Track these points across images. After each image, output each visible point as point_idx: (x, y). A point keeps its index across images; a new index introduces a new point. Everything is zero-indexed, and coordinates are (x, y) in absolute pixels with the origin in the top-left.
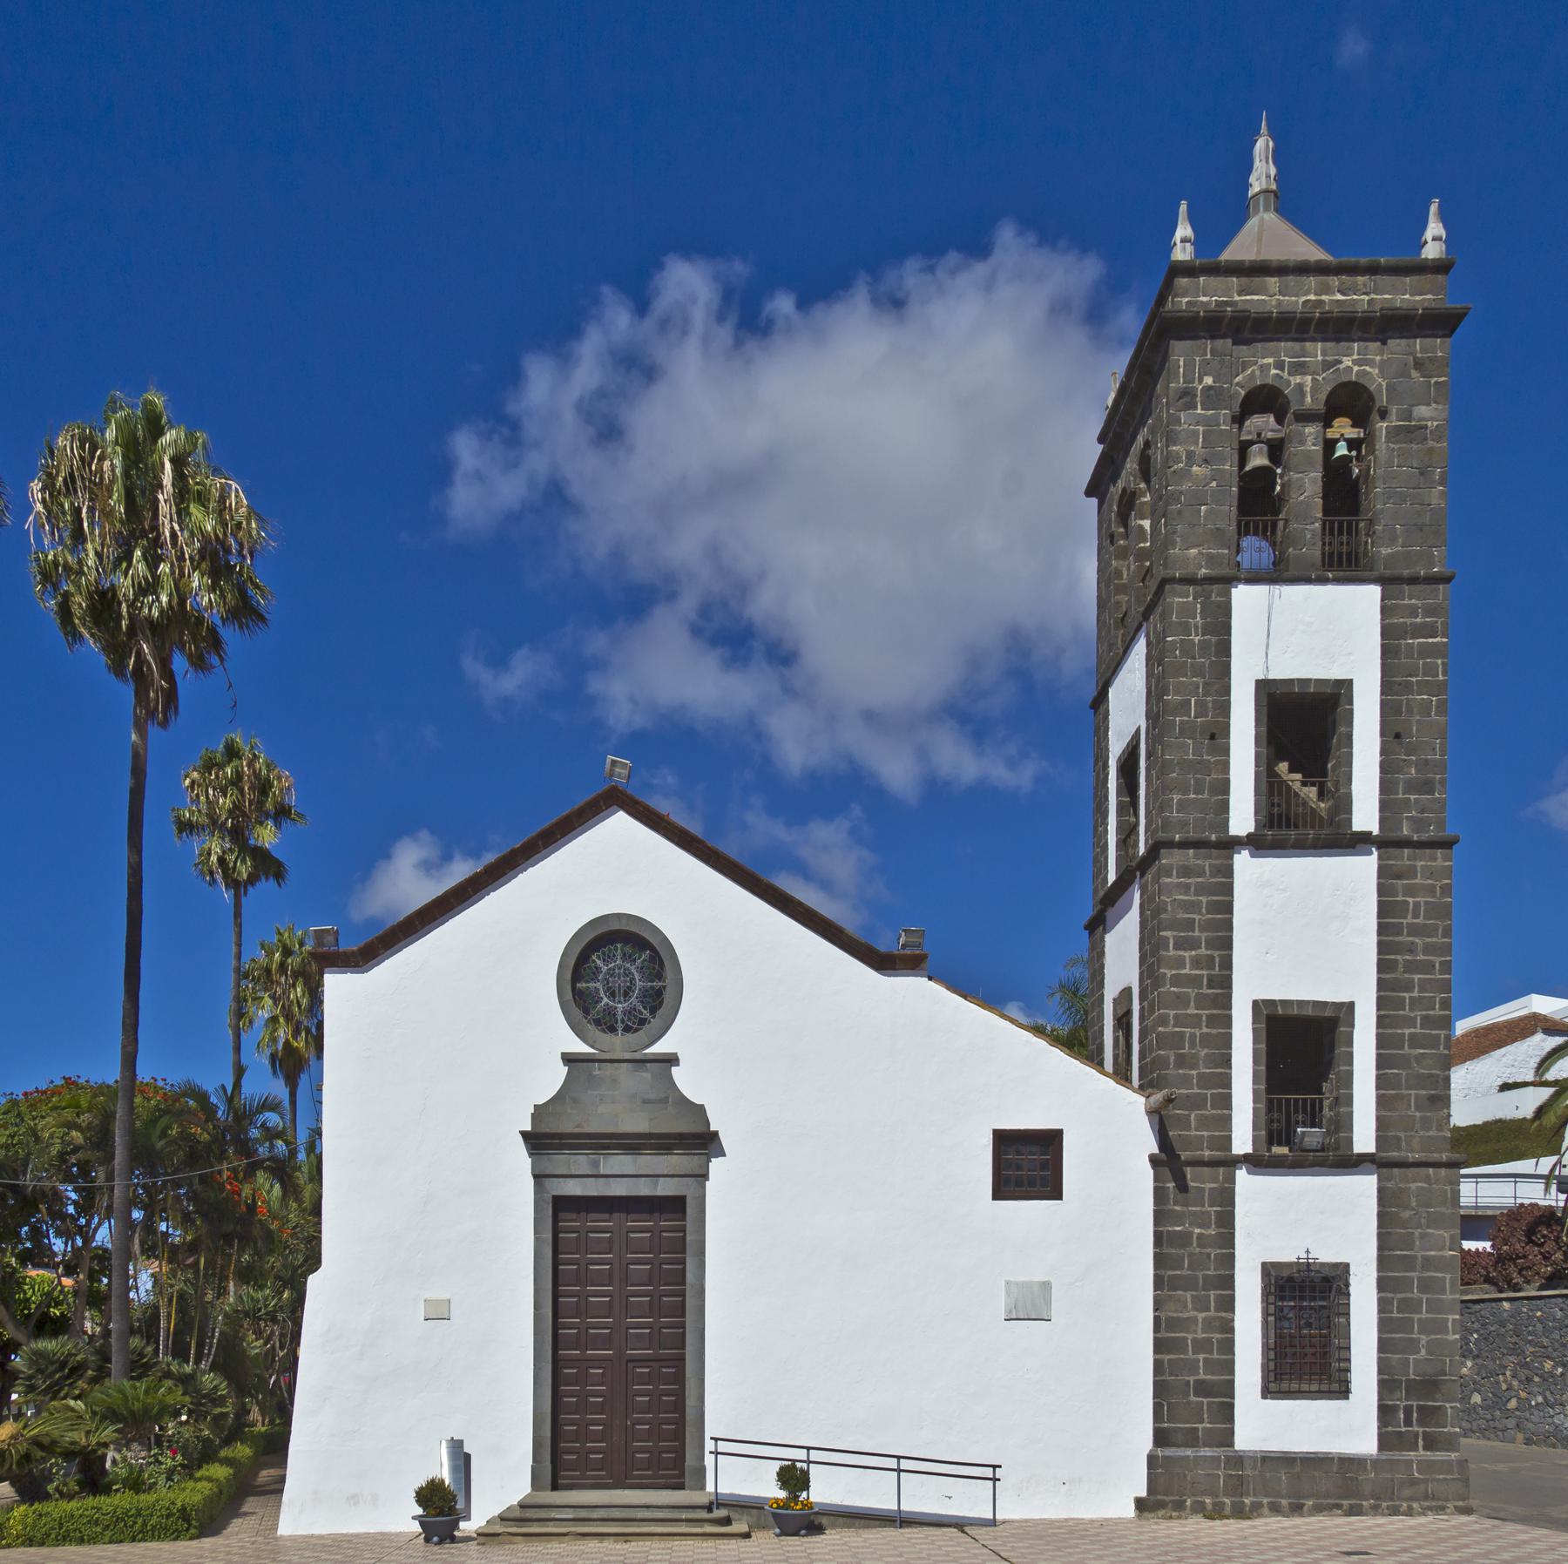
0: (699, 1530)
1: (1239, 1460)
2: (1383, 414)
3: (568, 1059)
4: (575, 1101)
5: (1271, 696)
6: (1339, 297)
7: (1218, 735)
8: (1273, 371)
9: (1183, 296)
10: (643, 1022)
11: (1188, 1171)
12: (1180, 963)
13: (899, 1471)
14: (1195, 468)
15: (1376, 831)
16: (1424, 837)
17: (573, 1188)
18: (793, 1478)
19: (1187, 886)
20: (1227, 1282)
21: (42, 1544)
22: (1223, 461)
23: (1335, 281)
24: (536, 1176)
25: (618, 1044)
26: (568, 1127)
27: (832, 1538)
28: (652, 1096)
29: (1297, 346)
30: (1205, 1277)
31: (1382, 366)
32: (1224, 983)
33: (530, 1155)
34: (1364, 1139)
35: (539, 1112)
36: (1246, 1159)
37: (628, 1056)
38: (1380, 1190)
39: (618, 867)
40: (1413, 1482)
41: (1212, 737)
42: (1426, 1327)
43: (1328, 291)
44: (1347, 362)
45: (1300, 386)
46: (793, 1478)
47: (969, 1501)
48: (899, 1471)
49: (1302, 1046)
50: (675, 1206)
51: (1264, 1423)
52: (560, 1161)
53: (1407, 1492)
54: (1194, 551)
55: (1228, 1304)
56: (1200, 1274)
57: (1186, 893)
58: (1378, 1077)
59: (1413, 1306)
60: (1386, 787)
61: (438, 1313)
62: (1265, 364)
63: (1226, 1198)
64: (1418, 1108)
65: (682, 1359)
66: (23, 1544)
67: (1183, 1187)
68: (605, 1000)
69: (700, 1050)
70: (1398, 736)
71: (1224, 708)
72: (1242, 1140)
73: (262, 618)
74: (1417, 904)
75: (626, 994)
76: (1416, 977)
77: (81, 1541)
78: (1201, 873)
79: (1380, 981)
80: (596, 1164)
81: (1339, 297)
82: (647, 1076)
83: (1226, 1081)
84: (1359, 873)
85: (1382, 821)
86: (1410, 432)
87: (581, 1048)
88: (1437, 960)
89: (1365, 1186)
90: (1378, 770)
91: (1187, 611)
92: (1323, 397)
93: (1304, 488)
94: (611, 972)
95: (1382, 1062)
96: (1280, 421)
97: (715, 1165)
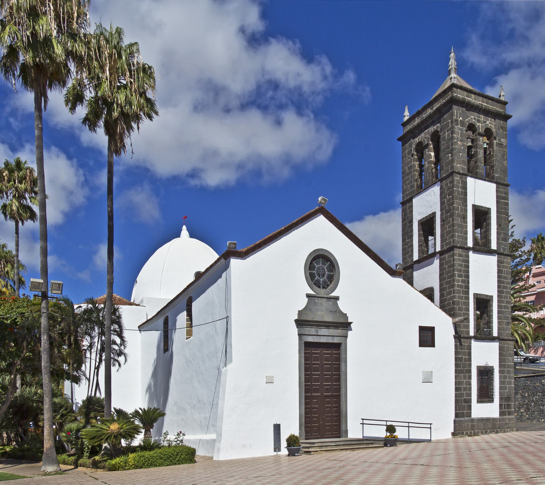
0: (364, 446)
1: (473, 420)
2: (495, 138)
3: (308, 296)
4: (310, 310)
10: (328, 285)
11: (49, 299)
13: (409, 427)
17: (310, 339)
18: (391, 429)
19: (460, 259)
21: (141, 468)
24: (299, 335)
25: (322, 292)
26: (309, 319)
27: (401, 447)
28: (332, 310)
31: (495, 125)
33: (297, 327)
34: (495, 334)
37: (326, 296)
38: (500, 347)
39: (319, 234)
40: (507, 424)
46: (391, 429)
47: (423, 434)
48: (409, 427)
51: (481, 411)
53: (506, 427)
54: (459, 165)
55: (470, 377)
60: (498, 239)
61: (270, 381)
62: (472, 117)
63: (469, 348)
65: (339, 396)
66: (134, 468)
67: (461, 345)
68: (317, 277)
71: (466, 211)
75: (323, 276)
77: (156, 466)
79: (498, 291)
80: (317, 331)
82: (331, 303)
84: (493, 260)
86: (500, 145)
87: (312, 292)
89: (495, 345)
90: (496, 234)
91: (458, 182)
92: (483, 130)
94: (318, 268)
96: (473, 134)
97: (350, 333)
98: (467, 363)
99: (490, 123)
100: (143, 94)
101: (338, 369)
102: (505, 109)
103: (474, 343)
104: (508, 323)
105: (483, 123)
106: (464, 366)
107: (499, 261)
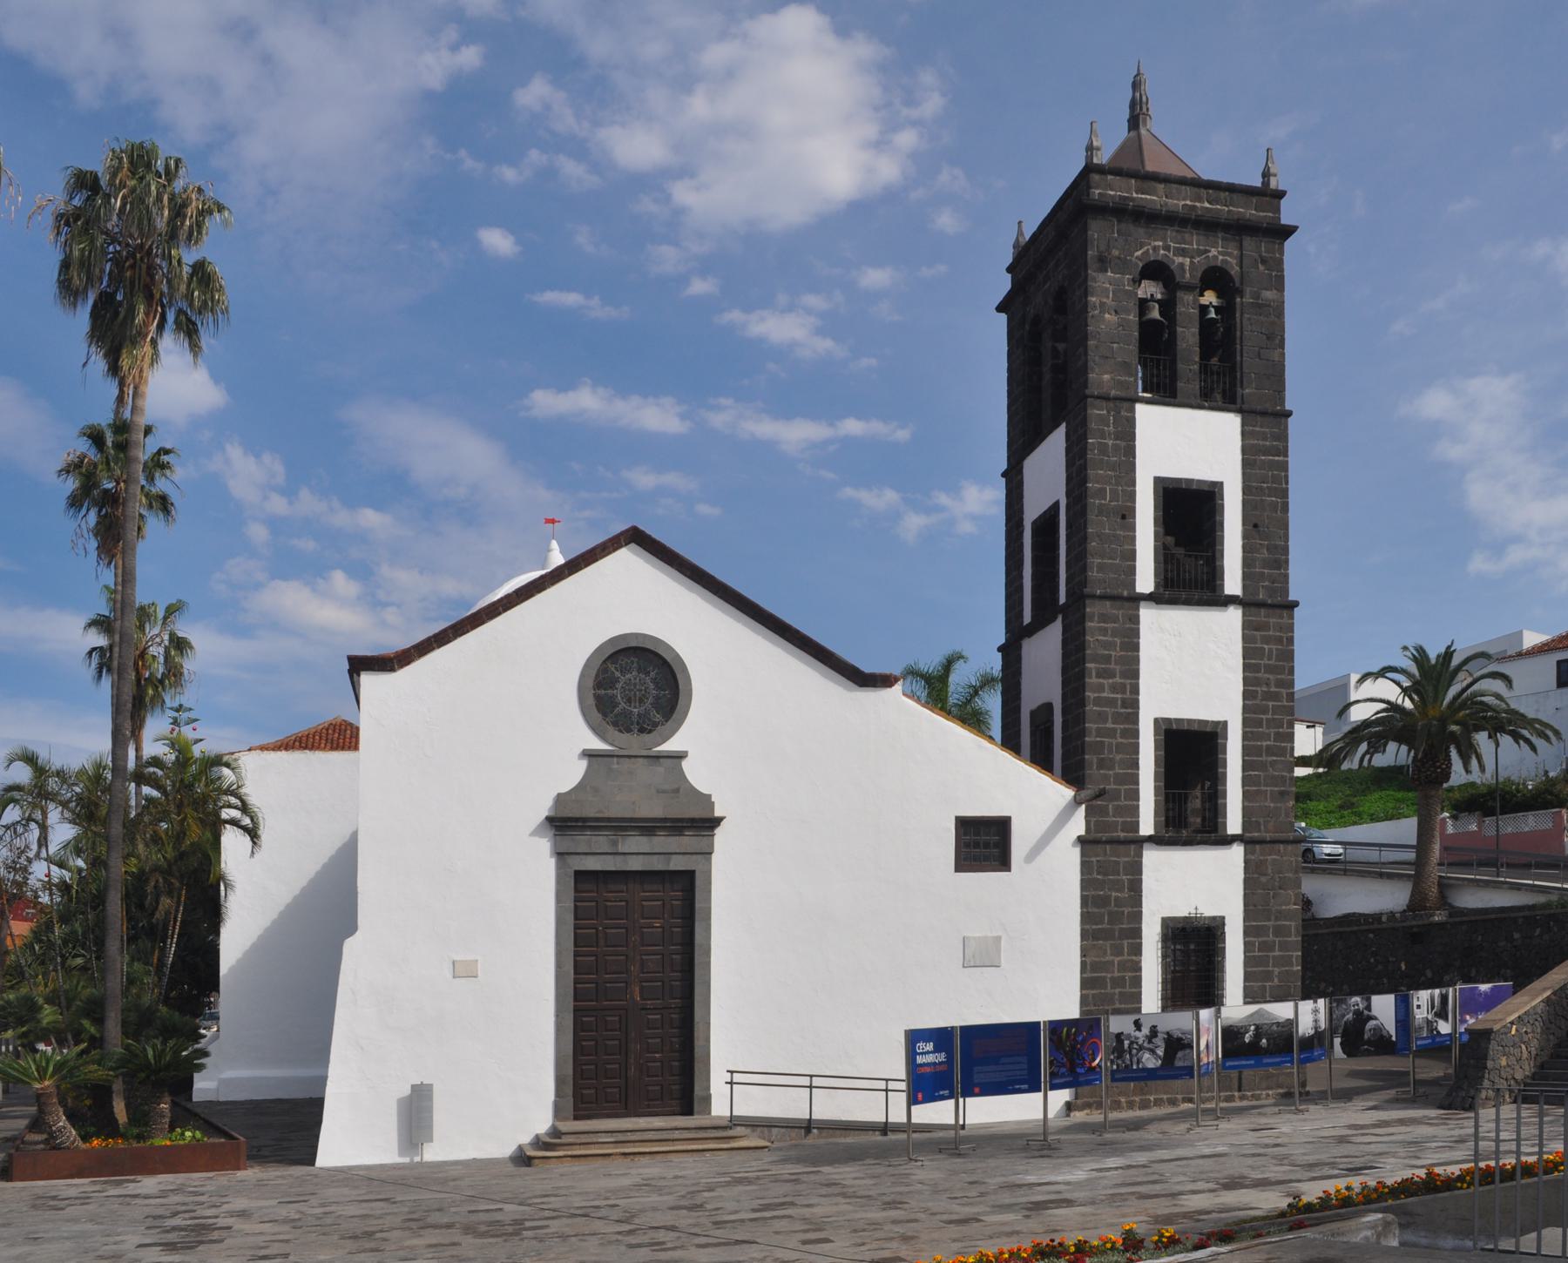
7: (1127, 515)
12: (1101, 688)
20: (1136, 933)
23: (1203, 192)
25: (633, 742)
35: (560, 799)
36: (1150, 839)
41: (1124, 517)
43: (1200, 200)
44: (1213, 252)
45: (1182, 265)
49: (1190, 749)
50: (690, 875)
52: (582, 841)
54: (1106, 377)
55: (1137, 950)
61: (464, 971)
62: (1157, 246)
69: (704, 747)
72: (1147, 827)
75: (641, 701)
80: (615, 843)
87: (598, 744)
88: (1284, 691)
93: (1188, 336)
95: (1246, 766)
99: (1219, 253)
102: (1277, 210)
103: (1151, 619)
104: (1282, 793)
105: (1189, 255)
106: (1115, 918)
107: (1246, 625)
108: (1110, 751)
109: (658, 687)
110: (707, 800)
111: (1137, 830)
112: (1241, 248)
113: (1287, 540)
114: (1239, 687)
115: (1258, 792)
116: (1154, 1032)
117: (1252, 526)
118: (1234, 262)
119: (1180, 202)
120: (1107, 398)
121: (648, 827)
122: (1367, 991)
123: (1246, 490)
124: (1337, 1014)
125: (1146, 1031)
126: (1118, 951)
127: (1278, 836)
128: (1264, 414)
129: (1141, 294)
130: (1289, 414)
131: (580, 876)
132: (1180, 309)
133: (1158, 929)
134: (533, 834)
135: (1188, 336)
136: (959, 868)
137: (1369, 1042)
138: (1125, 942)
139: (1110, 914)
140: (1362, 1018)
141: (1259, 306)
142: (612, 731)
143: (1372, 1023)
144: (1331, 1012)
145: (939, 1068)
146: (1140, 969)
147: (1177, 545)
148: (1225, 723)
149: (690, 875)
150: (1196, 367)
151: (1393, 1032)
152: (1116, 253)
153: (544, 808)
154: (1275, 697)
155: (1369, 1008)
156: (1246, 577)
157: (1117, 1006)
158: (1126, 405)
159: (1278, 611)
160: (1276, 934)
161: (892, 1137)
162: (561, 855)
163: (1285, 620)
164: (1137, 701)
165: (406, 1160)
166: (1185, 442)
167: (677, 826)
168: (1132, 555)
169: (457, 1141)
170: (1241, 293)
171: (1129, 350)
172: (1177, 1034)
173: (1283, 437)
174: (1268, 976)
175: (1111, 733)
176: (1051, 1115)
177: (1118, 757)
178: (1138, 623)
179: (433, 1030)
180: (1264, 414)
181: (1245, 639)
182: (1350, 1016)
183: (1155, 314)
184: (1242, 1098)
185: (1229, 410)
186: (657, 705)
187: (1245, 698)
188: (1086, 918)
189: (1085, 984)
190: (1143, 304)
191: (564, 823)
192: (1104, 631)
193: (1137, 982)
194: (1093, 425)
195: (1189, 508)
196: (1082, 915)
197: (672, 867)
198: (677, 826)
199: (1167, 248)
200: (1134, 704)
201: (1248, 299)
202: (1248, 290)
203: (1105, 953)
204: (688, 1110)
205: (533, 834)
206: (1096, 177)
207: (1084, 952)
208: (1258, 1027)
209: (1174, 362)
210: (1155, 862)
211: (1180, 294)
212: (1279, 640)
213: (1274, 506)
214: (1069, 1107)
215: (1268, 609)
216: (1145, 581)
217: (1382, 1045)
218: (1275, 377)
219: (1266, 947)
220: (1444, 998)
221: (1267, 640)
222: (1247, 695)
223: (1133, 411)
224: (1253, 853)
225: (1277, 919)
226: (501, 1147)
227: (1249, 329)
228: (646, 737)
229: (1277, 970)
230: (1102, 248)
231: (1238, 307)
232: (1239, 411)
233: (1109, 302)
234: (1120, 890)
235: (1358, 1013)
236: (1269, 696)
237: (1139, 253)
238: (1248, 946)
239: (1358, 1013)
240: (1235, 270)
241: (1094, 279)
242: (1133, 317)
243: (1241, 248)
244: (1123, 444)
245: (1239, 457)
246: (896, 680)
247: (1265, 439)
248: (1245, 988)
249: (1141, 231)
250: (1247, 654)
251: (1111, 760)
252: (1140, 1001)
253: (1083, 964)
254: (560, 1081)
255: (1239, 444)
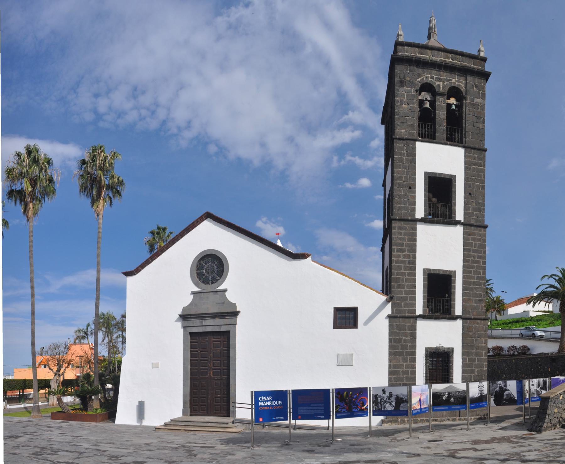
5: (429, 177)
6: (451, 60)
7: (412, 187)
8: (430, 79)
9: (400, 52)
12: (399, 256)
14: (404, 105)
15: (462, 221)
16: (478, 224)
20: (414, 353)
22: (414, 104)
23: (450, 55)
25: (209, 287)
29: (438, 73)
30: (406, 352)
32: (413, 263)
35: (184, 309)
36: (420, 316)
41: (410, 188)
42: (477, 366)
43: (448, 58)
44: (453, 81)
45: (439, 85)
49: (439, 283)
50: (228, 333)
52: (191, 322)
54: (403, 131)
55: (414, 360)
56: (405, 351)
57: (401, 235)
58: (463, 294)
59: (474, 360)
61: (155, 366)
62: (428, 76)
64: (475, 303)
69: (232, 287)
70: (470, 194)
72: (419, 310)
73: (120, 195)
74: (476, 244)
75: (212, 272)
76: (475, 265)
78: (406, 229)
80: (202, 322)
81: (451, 60)
83: (414, 293)
85: (465, 218)
87: (196, 289)
88: (481, 260)
93: (441, 115)
95: (464, 289)
98: (410, 370)
99: (456, 81)
100: (154, 238)
101: (229, 357)
102: (484, 66)
103: (421, 228)
104: (480, 301)
105: (442, 81)
106: (404, 347)
107: (465, 233)
108: (403, 281)
109: (218, 267)
110: (234, 305)
111: (415, 313)
112: (466, 80)
113: (484, 201)
114: (462, 258)
115: (469, 299)
116: (391, 395)
117: (468, 194)
118: (463, 85)
119: (439, 58)
120: (403, 139)
121: (213, 316)
122: (505, 380)
123: (466, 179)
124: (492, 388)
125: (387, 394)
126: (405, 360)
127: (479, 317)
128: (475, 149)
129: (420, 98)
130: (485, 150)
131: (191, 334)
132: (438, 103)
133: (423, 352)
134: (176, 321)
135: (441, 115)
136: (336, 326)
137: (506, 400)
138: (409, 357)
139: (402, 345)
140: (503, 390)
141: (474, 105)
142: (202, 285)
143: (506, 392)
144: (489, 387)
145: (279, 407)
146: (415, 368)
147: (434, 197)
148: (455, 272)
149: (228, 333)
150: (445, 128)
151: (516, 396)
152: (408, 79)
153: (180, 312)
154: (478, 262)
155: (506, 386)
156: (465, 214)
157: (405, 382)
158: (412, 142)
159: (479, 228)
160: (476, 355)
161: (298, 431)
162: (184, 327)
163: (482, 232)
164: (415, 261)
165: (139, 424)
166: (438, 158)
167: (223, 315)
168: (414, 203)
169: (155, 419)
170: (465, 98)
171: (414, 120)
172: (400, 396)
173: (483, 159)
174: (472, 372)
175: (404, 274)
176: (372, 424)
177: (407, 284)
178: (416, 230)
179: (153, 386)
180: (475, 149)
181: (464, 238)
182: (498, 389)
183: (427, 105)
184: (459, 420)
185: (459, 146)
186: (217, 274)
187: (464, 262)
188: (391, 347)
189: (390, 373)
190: (421, 103)
191: (185, 317)
192: (401, 234)
193: (414, 373)
194: (396, 150)
195: (440, 187)
196: (389, 346)
197: (222, 330)
198: (223, 315)
199: (432, 78)
200: (414, 263)
201: (468, 101)
202: (469, 98)
203: (399, 361)
204: (228, 416)
205: (176, 321)
206: (399, 48)
207: (390, 361)
208: (449, 393)
209: (435, 126)
210: (421, 325)
211: (437, 97)
212: (480, 240)
213: (478, 187)
214: (383, 422)
215: (475, 227)
216: (420, 213)
217: (511, 401)
218: (481, 134)
219: (471, 360)
220: (545, 382)
221: (474, 239)
222: (464, 261)
223: (415, 144)
224: (466, 323)
225: (476, 349)
226: (159, 423)
227: (469, 114)
228: (214, 285)
229: (476, 370)
230: (402, 77)
231: (464, 104)
232: (463, 147)
233: (405, 100)
234: (407, 336)
235: (501, 388)
236: (474, 262)
237: (419, 79)
238: (464, 360)
239: (501, 388)
240: (463, 89)
241: (398, 90)
242: (416, 106)
243: (466, 80)
244: (410, 158)
245: (463, 166)
246: (308, 256)
247: (475, 159)
248: (462, 376)
249: (420, 70)
250: (465, 244)
251: (403, 285)
252: (415, 380)
253: (390, 366)
254: (185, 403)
255: (463, 160)
